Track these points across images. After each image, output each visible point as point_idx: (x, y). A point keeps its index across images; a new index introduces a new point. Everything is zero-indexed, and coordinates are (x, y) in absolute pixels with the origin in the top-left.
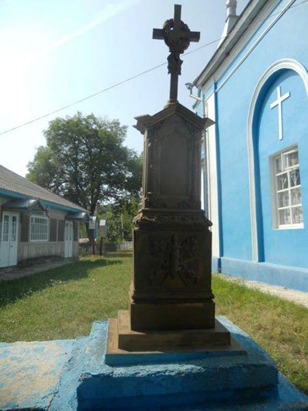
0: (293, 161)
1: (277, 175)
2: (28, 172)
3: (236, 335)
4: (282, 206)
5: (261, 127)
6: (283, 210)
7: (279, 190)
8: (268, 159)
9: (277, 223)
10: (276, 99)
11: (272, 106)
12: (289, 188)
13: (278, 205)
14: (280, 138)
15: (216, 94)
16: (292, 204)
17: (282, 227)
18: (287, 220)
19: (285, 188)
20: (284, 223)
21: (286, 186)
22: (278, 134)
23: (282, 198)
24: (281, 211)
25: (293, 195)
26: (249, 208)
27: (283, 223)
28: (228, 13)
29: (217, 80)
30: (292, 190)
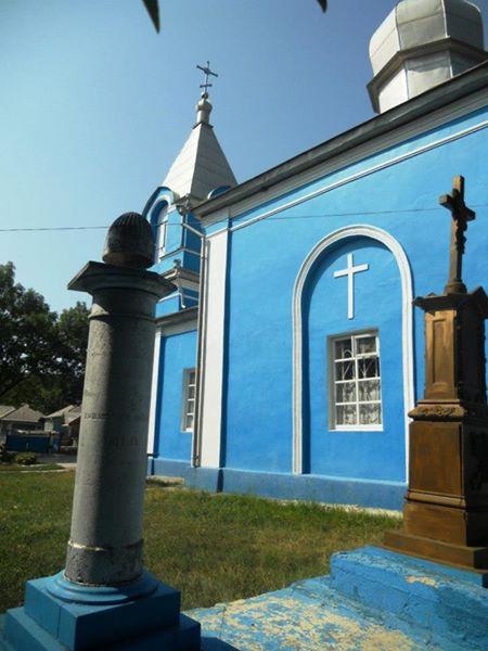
0: (363, 347)
1: (337, 361)
2: (52, 310)
3: (266, 591)
4: (340, 400)
5: (315, 297)
6: (343, 406)
7: (337, 358)
8: (325, 339)
9: (333, 422)
10: (345, 267)
11: (337, 274)
12: (356, 380)
13: (335, 376)
14: (350, 316)
15: (230, 234)
16: (362, 399)
17: (340, 428)
18: (347, 418)
19: (346, 379)
20: (341, 423)
21: (349, 376)
22: (347, 293)
23: (341, 392)
24: (338, 385)
25: (361, 389)
26: (291, 418)
27: (340, 422)
28: (199, 120)
29: (233, 215)
30: (360, 383)
